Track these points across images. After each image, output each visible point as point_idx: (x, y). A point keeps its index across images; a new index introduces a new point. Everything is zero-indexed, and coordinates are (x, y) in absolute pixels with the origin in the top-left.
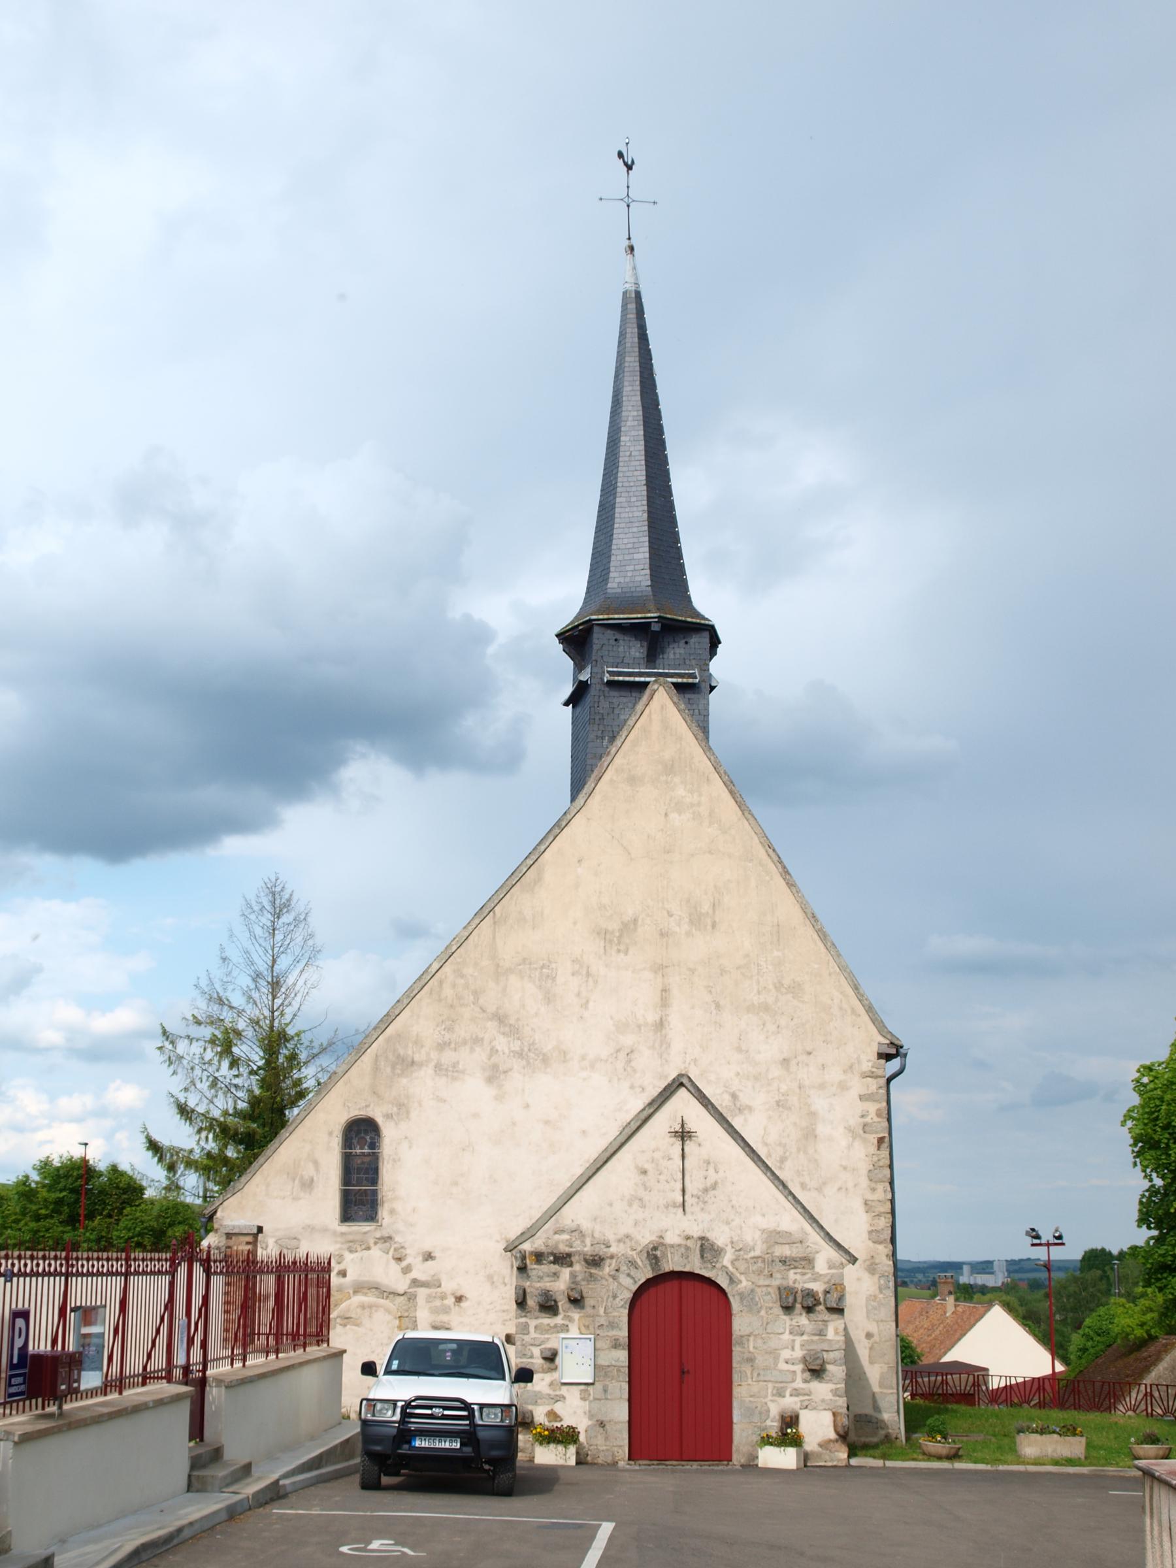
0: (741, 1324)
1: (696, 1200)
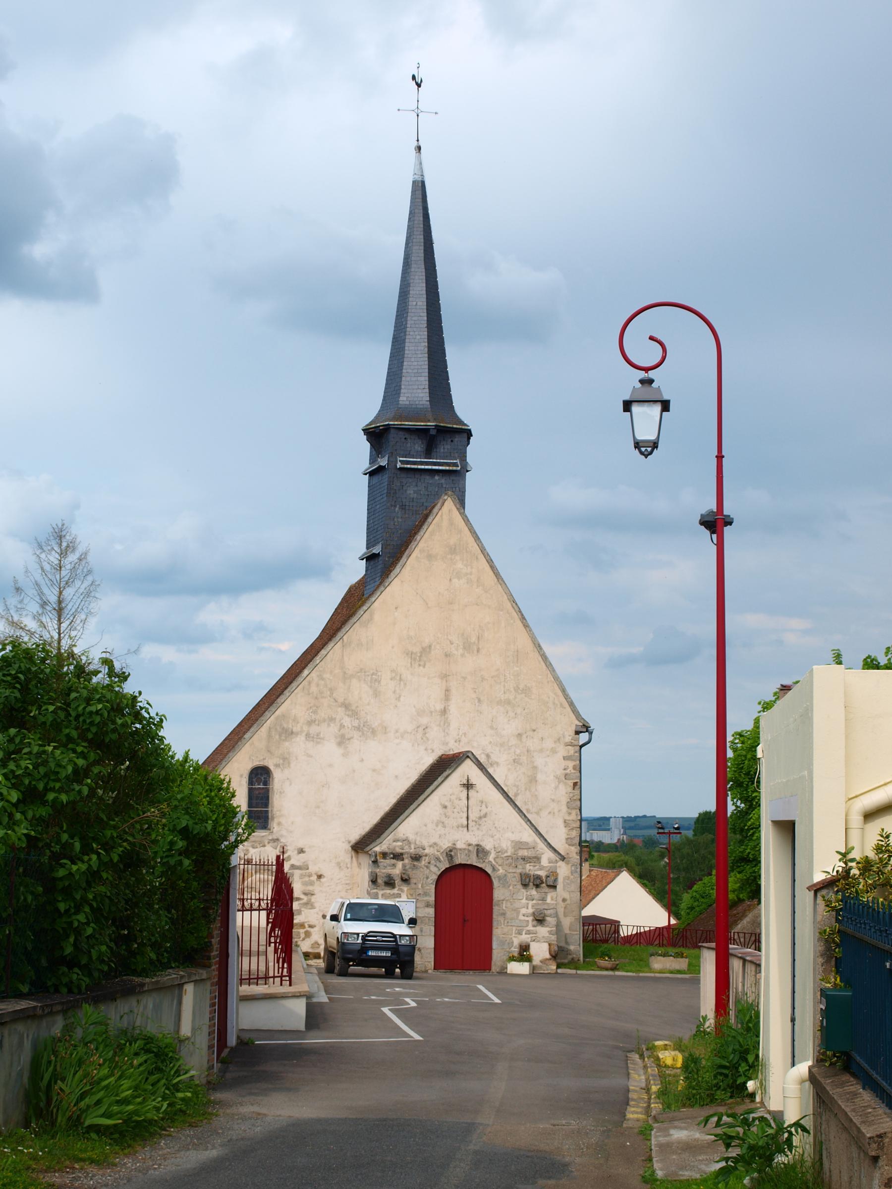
0: (498, 893)
1: (475, 823)
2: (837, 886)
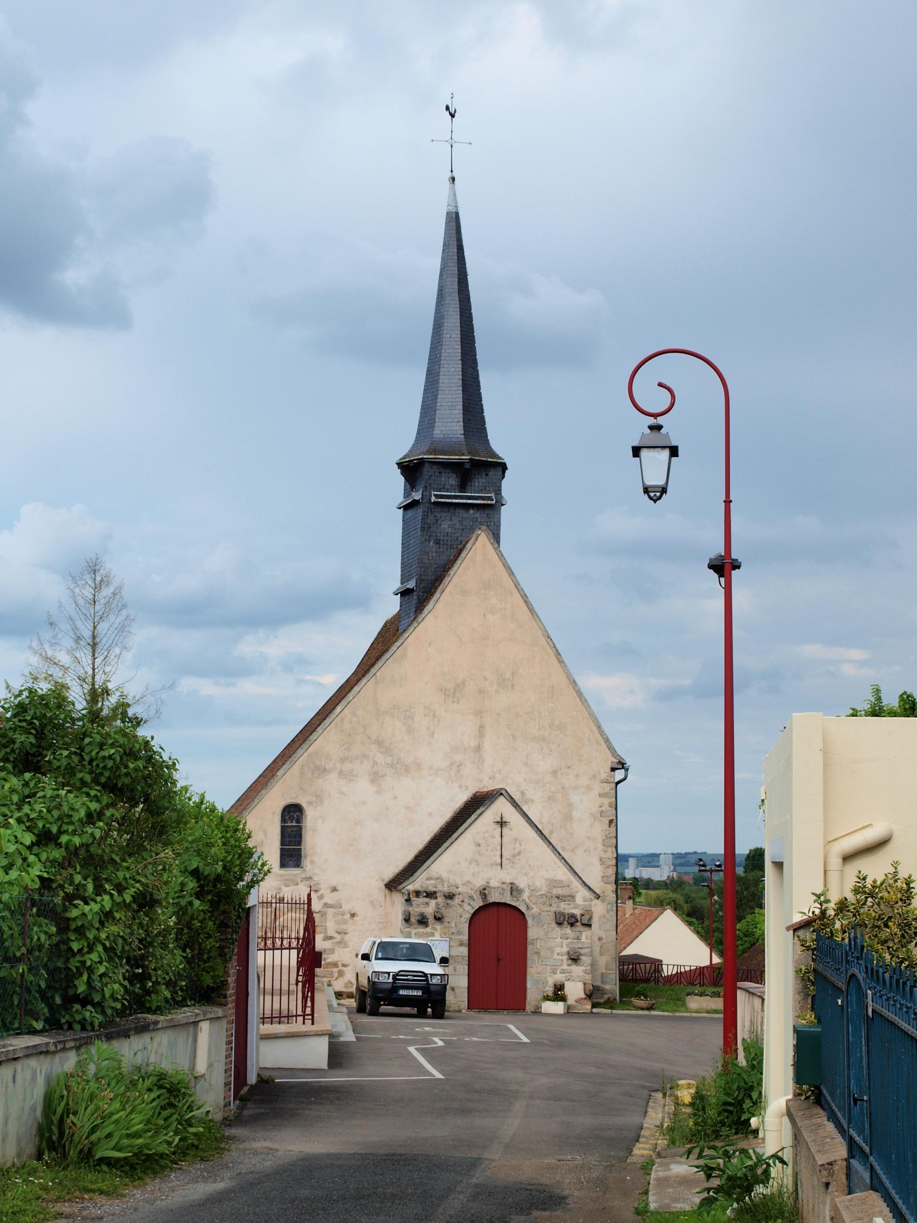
0: (533, 932)
2: (814, 926)
